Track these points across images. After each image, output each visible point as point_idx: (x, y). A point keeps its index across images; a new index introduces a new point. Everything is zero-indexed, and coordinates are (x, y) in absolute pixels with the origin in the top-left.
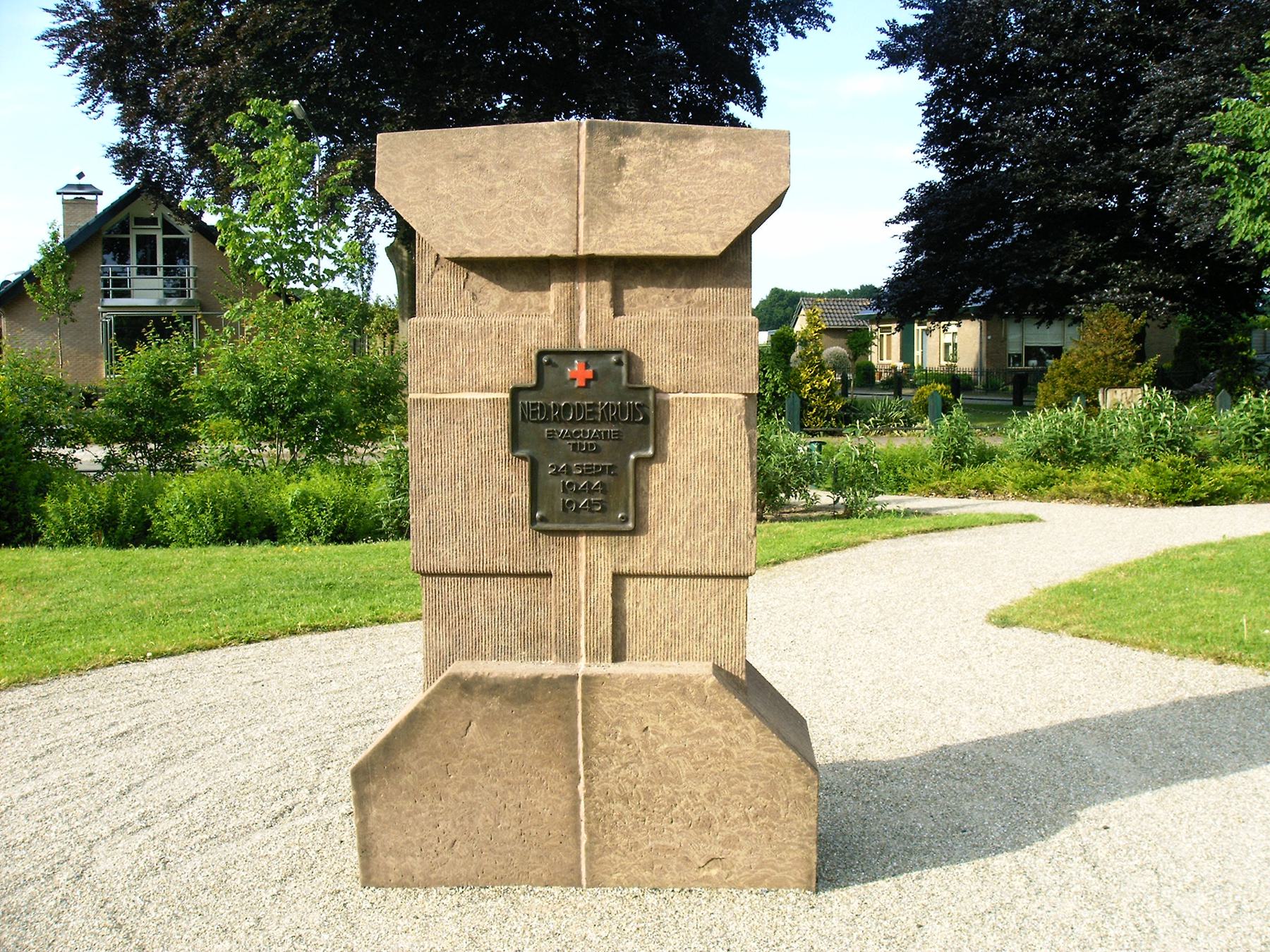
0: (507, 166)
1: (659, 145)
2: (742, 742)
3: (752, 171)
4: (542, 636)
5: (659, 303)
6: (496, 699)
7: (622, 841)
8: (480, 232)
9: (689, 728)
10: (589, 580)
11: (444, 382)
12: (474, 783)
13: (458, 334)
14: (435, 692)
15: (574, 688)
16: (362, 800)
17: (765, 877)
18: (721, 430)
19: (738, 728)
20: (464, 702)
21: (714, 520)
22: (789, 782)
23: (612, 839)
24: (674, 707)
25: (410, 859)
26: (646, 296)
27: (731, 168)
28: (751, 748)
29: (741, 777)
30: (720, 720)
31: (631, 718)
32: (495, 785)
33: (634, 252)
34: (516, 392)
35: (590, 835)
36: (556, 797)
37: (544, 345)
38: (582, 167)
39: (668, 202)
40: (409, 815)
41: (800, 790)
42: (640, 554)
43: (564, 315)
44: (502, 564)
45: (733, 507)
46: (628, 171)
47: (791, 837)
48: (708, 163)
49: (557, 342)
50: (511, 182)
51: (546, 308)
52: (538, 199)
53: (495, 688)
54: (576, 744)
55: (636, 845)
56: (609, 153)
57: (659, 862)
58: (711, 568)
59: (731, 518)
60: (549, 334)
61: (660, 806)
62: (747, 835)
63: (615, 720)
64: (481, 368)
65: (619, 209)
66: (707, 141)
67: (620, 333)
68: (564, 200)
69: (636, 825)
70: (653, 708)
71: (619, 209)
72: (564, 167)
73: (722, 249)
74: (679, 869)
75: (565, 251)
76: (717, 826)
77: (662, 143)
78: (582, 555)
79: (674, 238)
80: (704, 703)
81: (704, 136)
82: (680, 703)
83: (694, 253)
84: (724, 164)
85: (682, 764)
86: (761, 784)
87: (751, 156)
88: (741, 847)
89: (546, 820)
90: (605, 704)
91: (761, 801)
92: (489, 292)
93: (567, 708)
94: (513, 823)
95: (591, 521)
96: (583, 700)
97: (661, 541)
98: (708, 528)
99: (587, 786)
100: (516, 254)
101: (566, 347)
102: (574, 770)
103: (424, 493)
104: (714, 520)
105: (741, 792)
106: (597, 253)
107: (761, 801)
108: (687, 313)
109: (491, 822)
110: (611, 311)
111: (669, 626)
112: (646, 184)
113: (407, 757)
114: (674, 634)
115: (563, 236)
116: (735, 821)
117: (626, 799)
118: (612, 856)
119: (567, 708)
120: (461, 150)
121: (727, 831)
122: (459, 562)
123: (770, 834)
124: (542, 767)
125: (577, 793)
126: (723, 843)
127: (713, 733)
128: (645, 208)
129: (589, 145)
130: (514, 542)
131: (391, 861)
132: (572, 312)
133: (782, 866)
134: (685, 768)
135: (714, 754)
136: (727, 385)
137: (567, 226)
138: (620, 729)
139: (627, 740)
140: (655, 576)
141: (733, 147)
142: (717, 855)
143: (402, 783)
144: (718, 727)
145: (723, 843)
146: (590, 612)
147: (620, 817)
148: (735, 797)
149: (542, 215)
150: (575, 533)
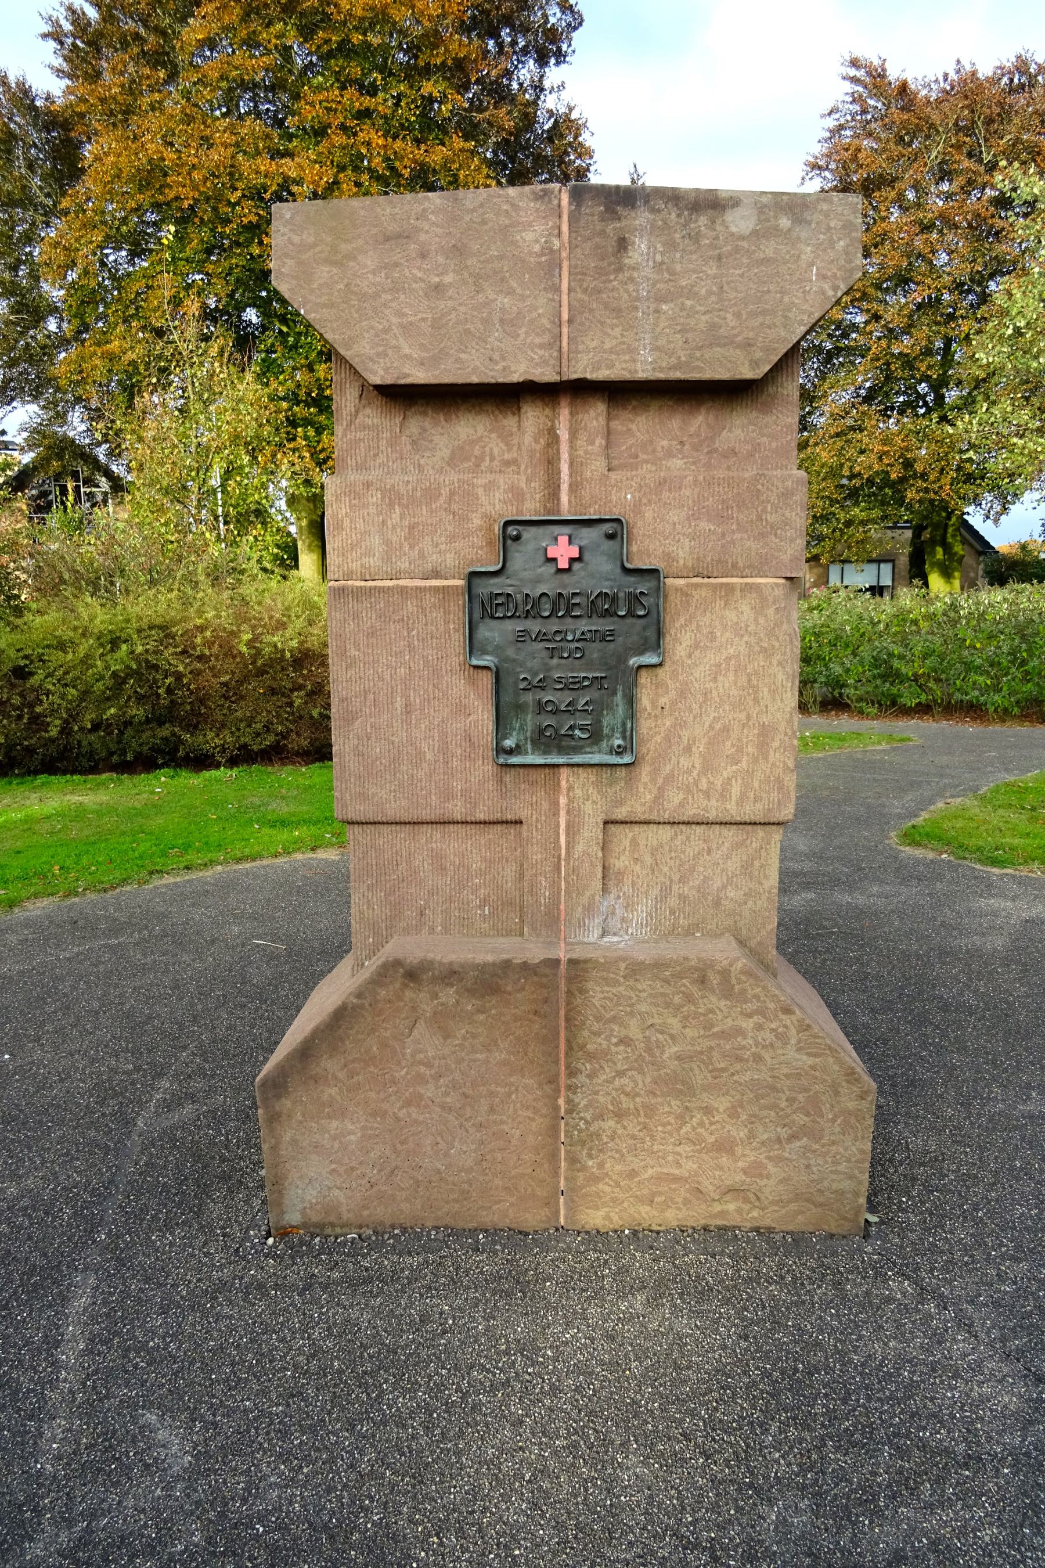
5: (669, 454)
10: (572, 830)
12: (421, 1097)
19: (773, 1026)
20: (408, 994)
21: (740, 750)
23: (601, 1165)
24: (689, 999)
27: (776, 251)
29: (774, 1089)
30: (750, 1016)
32: (448, 1100)
40: (334, 1138)
41: (851, 1105)
44: (457, 809)
55: (632, 1174)
57: (660, 1194)
59: (763, 746)
60: (518, 495)
64: (426, 544)
67: (619, 497)
70: (660, 1000)
75: (546, 375)
76: (739, 1150)
79: (698, 354)
80: (727, 992)
82: (697, 994)
86: (801, 1097)
89: (514, 1142)
90: (597, 993)
91: (800, 1119)
93: (546, 1001)
95: (576, 750)
97: (669, 779)
100: (475, 380)
103: (349, 719)
104: (740, 750)
105: (773, 1107)
106: (589, 376)
107: (800, 1119)
113: (329, 1065)
115: (541, 352)
116: (763, 1143)
118: (601, 1186)
119: (546, 1001)
124: (511, 1075)
127: (740, 1032)
133: (821, 1199)
135: (739, 1059)
148: (765, 1113)
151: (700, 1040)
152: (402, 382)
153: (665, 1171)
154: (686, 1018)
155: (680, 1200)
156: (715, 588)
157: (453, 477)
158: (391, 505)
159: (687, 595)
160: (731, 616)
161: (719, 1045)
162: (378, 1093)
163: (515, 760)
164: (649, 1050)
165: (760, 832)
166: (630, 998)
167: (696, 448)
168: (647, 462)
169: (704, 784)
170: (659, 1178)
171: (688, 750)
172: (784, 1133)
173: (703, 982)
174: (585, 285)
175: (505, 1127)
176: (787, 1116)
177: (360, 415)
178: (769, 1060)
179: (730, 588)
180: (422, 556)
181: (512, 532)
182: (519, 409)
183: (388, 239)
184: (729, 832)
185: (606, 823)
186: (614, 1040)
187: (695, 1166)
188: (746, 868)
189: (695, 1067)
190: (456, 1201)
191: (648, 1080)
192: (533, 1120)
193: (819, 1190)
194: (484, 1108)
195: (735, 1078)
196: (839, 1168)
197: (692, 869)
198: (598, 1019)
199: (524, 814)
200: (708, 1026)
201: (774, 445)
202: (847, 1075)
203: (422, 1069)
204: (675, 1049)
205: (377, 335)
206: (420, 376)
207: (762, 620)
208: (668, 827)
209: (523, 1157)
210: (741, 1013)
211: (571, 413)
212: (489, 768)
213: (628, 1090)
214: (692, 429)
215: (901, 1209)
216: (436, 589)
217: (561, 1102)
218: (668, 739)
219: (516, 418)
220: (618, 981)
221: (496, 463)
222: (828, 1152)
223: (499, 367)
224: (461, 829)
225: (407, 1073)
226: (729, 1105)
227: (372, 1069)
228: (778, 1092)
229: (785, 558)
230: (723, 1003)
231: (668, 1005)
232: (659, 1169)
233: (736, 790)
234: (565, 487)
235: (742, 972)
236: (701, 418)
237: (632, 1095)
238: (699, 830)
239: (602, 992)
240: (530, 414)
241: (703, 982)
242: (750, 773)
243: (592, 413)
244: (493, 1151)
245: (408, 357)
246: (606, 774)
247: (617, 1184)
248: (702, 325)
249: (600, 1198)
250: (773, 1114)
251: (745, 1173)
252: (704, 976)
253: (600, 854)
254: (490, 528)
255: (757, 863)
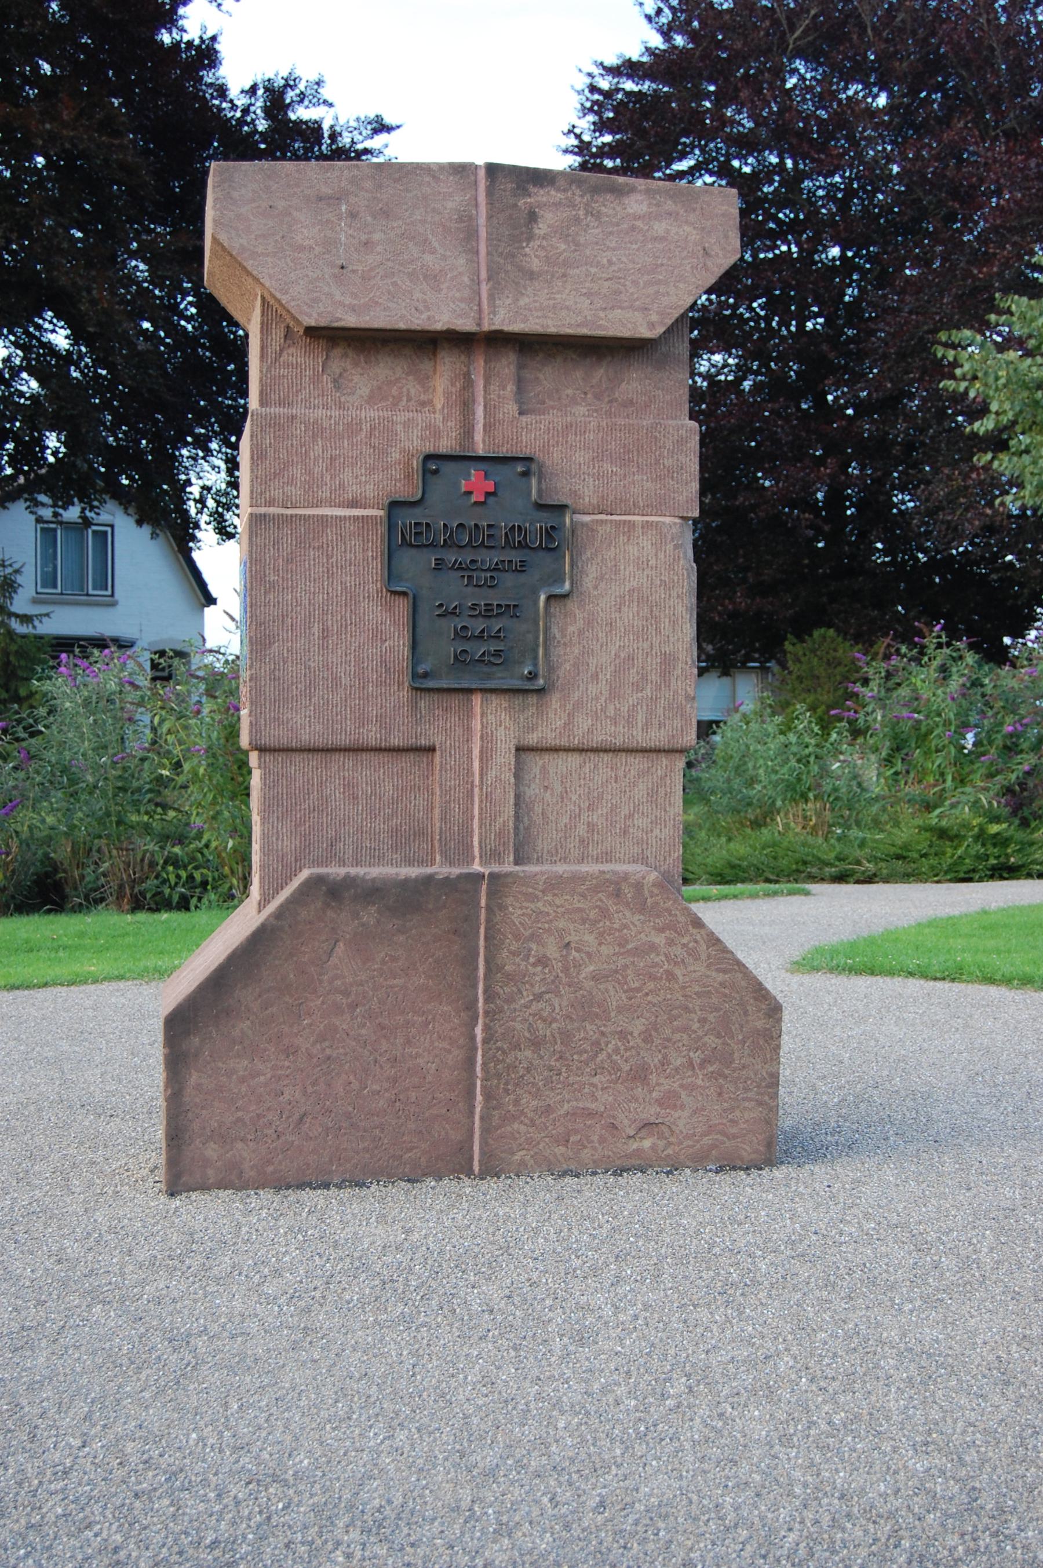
0: (386, 214)
1: (578, 199)
2: (689, 960)
3: (695, 236)
4: (421, 833)
5: (573, 401)
6: (372, 909)
7: (530, 1103)
8: (355, 296)
9: (623, 943)
10: (485, 757)
11: (295, 492)
13: (316, 430)
14: (279, 914)
15: (477, 892)
16: (177, 1061)
17: (714, 1146)
18: (653, 562)
19: (685, 941)
20: (330, 913)
21: (644, 678)
22: (746, 1013)
23: (517, 1102)
25: (240, 1145)
26: (557, 391)
27: (668, 231)
28: (700, 968)
29: (686, 1009)
30: (662, 930)
31: (549, 930)
32: (363, 1031)
33: (552, 330)
34: (394, 506)
35: (488, 1096)
36: (445, 1045)
37: (429, 448)
38: (482, 220)
39: (593, 270)
40: (242, 1080)
42: (551, 723)
43: (456, 411)
44: (372, 735)
45: (668, 661)
46: (541, 228)
47: (746, 1090)
48: (639, 224)
49: (446, 445)
50: (392, 234)
51: (430, 402)
52: (428, 258)
53: (372, 893)
54: (476, 968)
55: (548, 1110)
56: (516, 205)
57: (576, 1132)
58: (640, 738)
60: (437, 434)
61: (580, 1053)
62: (691, 1088)
63: (527, 934)
64: (347, 476)
65: (531, 275)
66: (635, 197)
67: (528, 435)
68: (462, 261)
69: (548, 1081)
71: (531, 275)
72: (460, 220)
73: (661, 330)
74: (602, 1140)
75: (466, 324)
76: (653, 1078)
77: (582, 196)
78: (477, 725)
79: (602, 314)
80: (642, 908)
81: (633, 190)
82: (613, 909)
83: (626, 334)
84: (660, 227)
85: (612, 993)
86: (711, 1017)
87: (692, 218)
88: (682, 1107)
89: (429, 1078)
90: (517, 911)
91: (711, 1040)
92: (356, 379)
93: (466, 919)
94: (386, 1085)
95: (489, 677)
96: (488, 908)
98: (638, 688)
99: (487, 1028)
100: (402, 326)
101: (458, 452)
102: (471, 1006)
104: (644, 678)
105: (685, 1029)
106: (506, 328)
108: (609, 414)
109: (355, 1085)
110: (516, 407)
111: (584, 817)
112: (563, 247)
113: (246, 996)
114: (591, 827)
115: (463, 305)
116: (677, 1069)
117: (536, 1044)
118: (516, 1126)
119: (466, 919)
120: (326, 190)
121: (666, 1085)
122: (310, 733)
123: (721, 1087)
125: (473, 1038)
126: (660, 1102)
127: (653, 947)
128: (564, 275)
129: (490, 193)
130: (387, 710)
131: (212, 1151)
132: (466, 406)
133: (734, 1130)
134: (616, 998)
135: (653, 978)
136: (658, 506)
137: (466, 293)
138: (534, 946)
139: (543, 961)
140: (567, 750)
141: (669, 205)
142: (652, 1120)
143: (236, 1033)
144: (660, 940)
145: (660, 1102)
146: (487, 797)
147: (528, 1070)
148: (677, 1036)
149: (433, 279)
150: (470, 691)
151: (614, 958)
152: (336, 325)
153: (581, 1105)
154: (601, 934)
155: (596, 1138)
156: (618, 524)
157: (371, 414)
158: (314, 437)
159: (593, 530)
160: (633, 550)
161: (633, 963)
162: (291, 1026)
163: (431, 684)
164: (566, 969)
165: (664, 760)
166: (548, 914)
167: (598, 397)
168: (553, 408)
169: (611, 712)
170: (572, 1114)
171: (595, 677)
172: (696, 1057)
173: (618, 896)
174: (500, 250)
175: (420, 1061)
176: (700, 1038)
177: (285, 353)
178: (681, 978)
179: (632, 525)
180: (342, 485)
181: (433, 463)
182: (435, 354)
183: (320, 199)
184: (637, 763)
185: (518, 749)
186: (532, 960)
187: (611, 1099)
188: (652, 794)
189: (610, 988)
190: (366, 1150)
191: (565, 1003)
192: (449, 1052)
193: (731, 1121)
194: (399, 1041)
195: (649, 998)
196: (749, 1095)
197: (600, 797)
198: (517, 937)
199: (437, 740)
200: (623, 943)
201: (668, 397)
202: (755, 991)
203: (339, 997)
204: (592, 968)
205: (311, 282)
206: (351, 320)
207: (661, 555)
208: (576, 755)
209: (438, 1095)
210: (654, 928)
211: (485, 362)
212: (405, 694)
213: (545, 1014)
214: (594, 381)
215: (805, 1485)
216: (356, 518)
217: (479, 1030)
218: (576, 665)
219: (432, 363)
220: (537, 897)
221: (413, 403)
222: (738, 1078)
223: (424, 316)
224: (375, 759)
225: (323, 1003)
226: (643, 1028)
227: (287, 999)
228: (690, 1012)
229: (682, 498)
230: (637, 917)
231: (584, 921)
232: (575, 1103)
233: (640, 718)
234: (479, 427)
235: (654, 885)
236: (602, 371)
237: (548, 1021)
238: (606, 757)
239: (521, 908)
240: (446, 360)
241: (618, 896)
242: (654, 700)
243: (504, 362)
244: (407, 1089)
245: (341, 304)
246: (518, 700)
247: (533, 1123)
248: (604, 291)
249: (516, 1139)
250: (685, 1036)
251: (660, 1105)
252: (619, 890)
253: (512, 780)
254: (408, 464)
255: (662, 791)
